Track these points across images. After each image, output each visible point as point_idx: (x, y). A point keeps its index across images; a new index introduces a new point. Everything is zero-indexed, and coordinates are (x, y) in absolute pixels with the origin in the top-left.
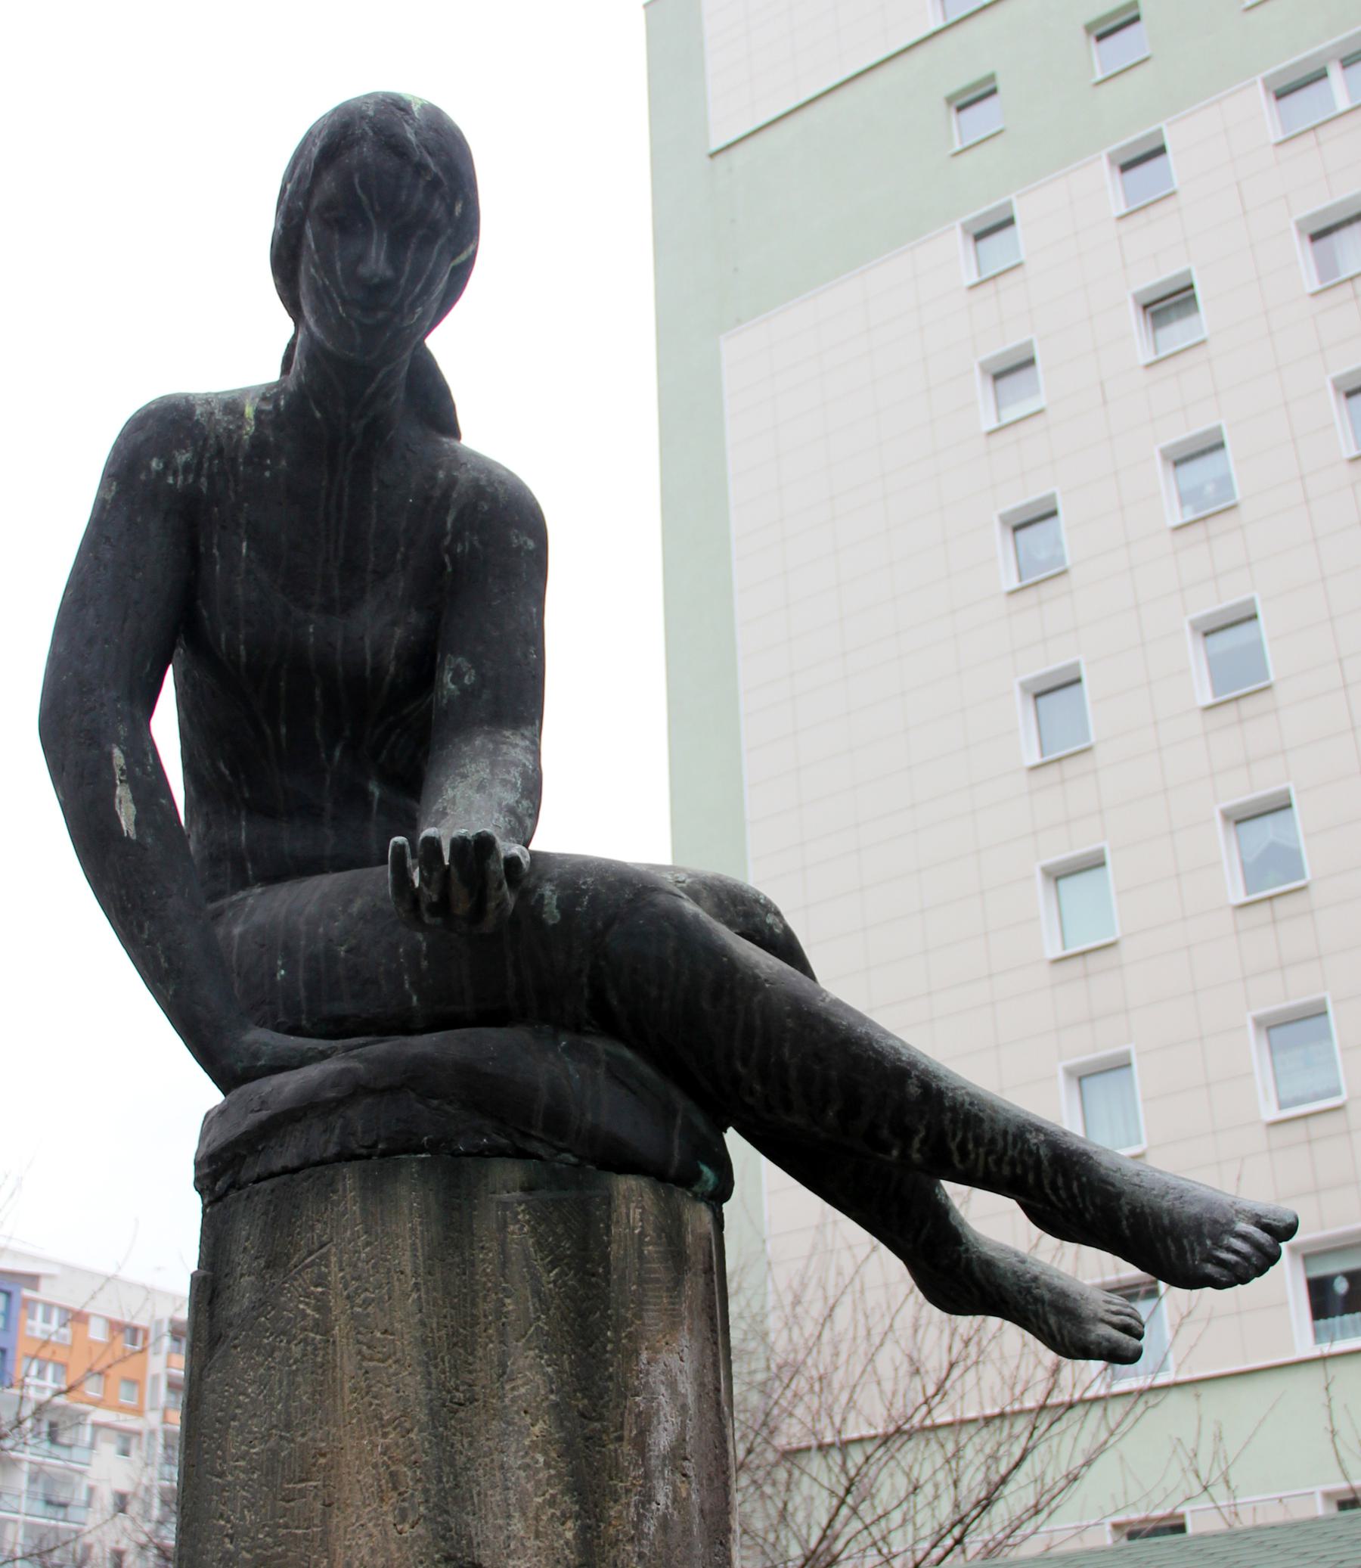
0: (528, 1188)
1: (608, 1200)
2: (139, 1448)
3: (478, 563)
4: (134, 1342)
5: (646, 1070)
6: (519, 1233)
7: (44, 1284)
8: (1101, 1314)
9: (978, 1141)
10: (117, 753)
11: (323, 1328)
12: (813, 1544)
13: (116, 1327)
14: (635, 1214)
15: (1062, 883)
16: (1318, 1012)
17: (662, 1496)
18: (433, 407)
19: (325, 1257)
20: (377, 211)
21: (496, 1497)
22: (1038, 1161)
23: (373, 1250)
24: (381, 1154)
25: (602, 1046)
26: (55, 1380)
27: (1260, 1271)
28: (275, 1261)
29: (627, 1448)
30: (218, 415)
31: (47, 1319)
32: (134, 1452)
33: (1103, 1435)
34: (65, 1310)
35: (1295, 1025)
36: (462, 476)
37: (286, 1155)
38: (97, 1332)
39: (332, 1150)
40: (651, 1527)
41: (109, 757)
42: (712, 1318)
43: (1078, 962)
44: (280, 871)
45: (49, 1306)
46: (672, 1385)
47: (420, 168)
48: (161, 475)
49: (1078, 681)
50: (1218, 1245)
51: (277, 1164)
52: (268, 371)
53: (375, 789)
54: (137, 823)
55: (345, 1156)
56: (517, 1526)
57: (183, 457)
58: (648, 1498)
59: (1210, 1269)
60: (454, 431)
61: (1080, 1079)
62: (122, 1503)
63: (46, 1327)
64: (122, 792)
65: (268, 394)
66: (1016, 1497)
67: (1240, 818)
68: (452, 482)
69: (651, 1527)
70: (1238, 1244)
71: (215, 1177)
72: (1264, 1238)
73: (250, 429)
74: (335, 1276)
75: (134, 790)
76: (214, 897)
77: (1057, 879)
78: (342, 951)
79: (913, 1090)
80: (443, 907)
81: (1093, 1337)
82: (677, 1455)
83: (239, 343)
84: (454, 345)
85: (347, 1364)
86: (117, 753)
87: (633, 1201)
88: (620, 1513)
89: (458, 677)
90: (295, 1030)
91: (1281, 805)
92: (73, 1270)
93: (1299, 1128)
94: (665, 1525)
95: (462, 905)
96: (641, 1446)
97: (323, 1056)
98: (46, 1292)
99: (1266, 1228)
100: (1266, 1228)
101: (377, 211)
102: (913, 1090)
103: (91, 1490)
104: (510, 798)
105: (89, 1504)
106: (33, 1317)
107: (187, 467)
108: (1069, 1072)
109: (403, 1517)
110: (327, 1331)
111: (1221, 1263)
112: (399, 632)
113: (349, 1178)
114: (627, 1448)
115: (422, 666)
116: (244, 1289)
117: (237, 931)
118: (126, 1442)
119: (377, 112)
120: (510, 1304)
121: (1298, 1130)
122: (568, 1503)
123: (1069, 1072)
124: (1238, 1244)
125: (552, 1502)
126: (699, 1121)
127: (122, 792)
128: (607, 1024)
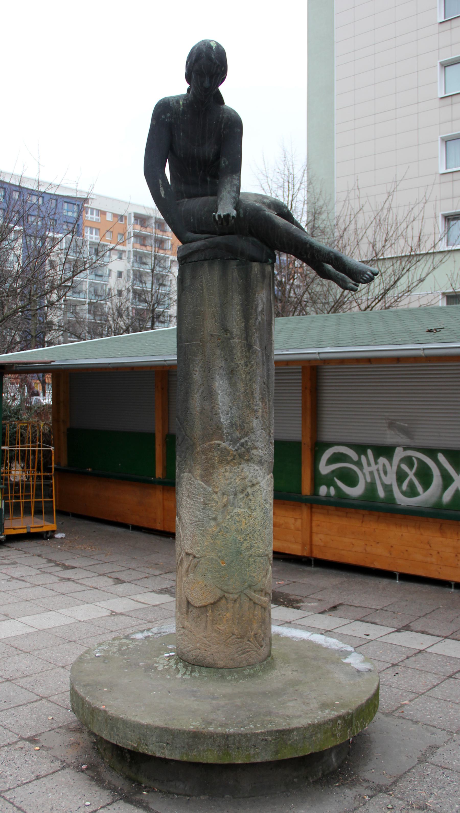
0: (237, 266)
1: (251, 267)
2: (125, 256)
3: (228, 132)
4: (122, 221)
5: (259, 242)
6: (235, 274)
7: (90, 201)
9: (320, 255)
10: (160, 181)
11: (202, 290)
12: (338, 297)
13: (115, 215)
14: (256, 269)
15: (447, 68)
17: (259, 319)
18: (219, 99)
19: (202, 278)
20: (207, 66)
21: (231, 319)
22: (332, 259)
23: (210, 278)
24: (211, 260)
25: (251, 238)
26: (96, 234)
28: (193, 277)
29: (253, 311)
30: (175, 104)
31: (92, 214)
32: (123, 258)
33: (431, 268)
34: (98, 211)
36: (225, 116)
37: (195, 258)
38: (109, 217)
39: (203, 258)
40: (257, 324)
41: (159, 182)
42: (270, 286)
43: (450, 99)
44: (190, 196)
45: (92, 209)
46: (262, 299)
47: (215, 63)
48: (164, 119)
50: (363, 276)
51: (193, 260)
52: (185, 92)
53: (209, 179)
54: (165, 195)
55: (205, 260)
56: (234, 324)
57: (168, 115)
58: (257, 319)
59: (361, 280)
60: (223, 103)
61: (446, 142)
62: (120, 274)
63: (92, 216)
64: (161, 188)
65: (185, 97)
66: (403, 284)
68: (223, 117)
69: (257, 324)
70: (367, 276)
71: (182, 261)
73: (182, 108)
74: (204, 281)
75: (164, 188)
76: (178, 200)
77: (445, 67)
78: (203, 218)
79: (308, 246)
80: (222, 224)
82: (262, 311)
83: (179, 87)
84: (222, 88)
85: (206, 296)
86: (160, 181)
87: (256, 267)
88: (252, 321)
89: (224, 163)
90: (195, 232)
92: (100, 196)
94: (260, 323)
95: (225, 224)
96: (256, 310)
97: (201, 239)
98: (91, 204)
101: (207, 66)
102: (308, 246)
103: (110, 271)
104: (234, 194)
105: (109, 275)
106: (87, 213)
107: (169, 117)
108: (442, 139)
109: (216, 322)
110: (203, 291)
111: (363, 279)
112: (213, 150)
113: (206, 264)
114: (253, 311)
115: (218, 156)
116: (188, 282)
117: (183, 209)
118: (121, 254)
119: (206, 50)
120: (234, 286)
122: (243, 320)
123: (442, 139)
124: (367, 276)
125: (240, 320)
126: (269, 251)
127: (161, 188)
128: (252, 234)
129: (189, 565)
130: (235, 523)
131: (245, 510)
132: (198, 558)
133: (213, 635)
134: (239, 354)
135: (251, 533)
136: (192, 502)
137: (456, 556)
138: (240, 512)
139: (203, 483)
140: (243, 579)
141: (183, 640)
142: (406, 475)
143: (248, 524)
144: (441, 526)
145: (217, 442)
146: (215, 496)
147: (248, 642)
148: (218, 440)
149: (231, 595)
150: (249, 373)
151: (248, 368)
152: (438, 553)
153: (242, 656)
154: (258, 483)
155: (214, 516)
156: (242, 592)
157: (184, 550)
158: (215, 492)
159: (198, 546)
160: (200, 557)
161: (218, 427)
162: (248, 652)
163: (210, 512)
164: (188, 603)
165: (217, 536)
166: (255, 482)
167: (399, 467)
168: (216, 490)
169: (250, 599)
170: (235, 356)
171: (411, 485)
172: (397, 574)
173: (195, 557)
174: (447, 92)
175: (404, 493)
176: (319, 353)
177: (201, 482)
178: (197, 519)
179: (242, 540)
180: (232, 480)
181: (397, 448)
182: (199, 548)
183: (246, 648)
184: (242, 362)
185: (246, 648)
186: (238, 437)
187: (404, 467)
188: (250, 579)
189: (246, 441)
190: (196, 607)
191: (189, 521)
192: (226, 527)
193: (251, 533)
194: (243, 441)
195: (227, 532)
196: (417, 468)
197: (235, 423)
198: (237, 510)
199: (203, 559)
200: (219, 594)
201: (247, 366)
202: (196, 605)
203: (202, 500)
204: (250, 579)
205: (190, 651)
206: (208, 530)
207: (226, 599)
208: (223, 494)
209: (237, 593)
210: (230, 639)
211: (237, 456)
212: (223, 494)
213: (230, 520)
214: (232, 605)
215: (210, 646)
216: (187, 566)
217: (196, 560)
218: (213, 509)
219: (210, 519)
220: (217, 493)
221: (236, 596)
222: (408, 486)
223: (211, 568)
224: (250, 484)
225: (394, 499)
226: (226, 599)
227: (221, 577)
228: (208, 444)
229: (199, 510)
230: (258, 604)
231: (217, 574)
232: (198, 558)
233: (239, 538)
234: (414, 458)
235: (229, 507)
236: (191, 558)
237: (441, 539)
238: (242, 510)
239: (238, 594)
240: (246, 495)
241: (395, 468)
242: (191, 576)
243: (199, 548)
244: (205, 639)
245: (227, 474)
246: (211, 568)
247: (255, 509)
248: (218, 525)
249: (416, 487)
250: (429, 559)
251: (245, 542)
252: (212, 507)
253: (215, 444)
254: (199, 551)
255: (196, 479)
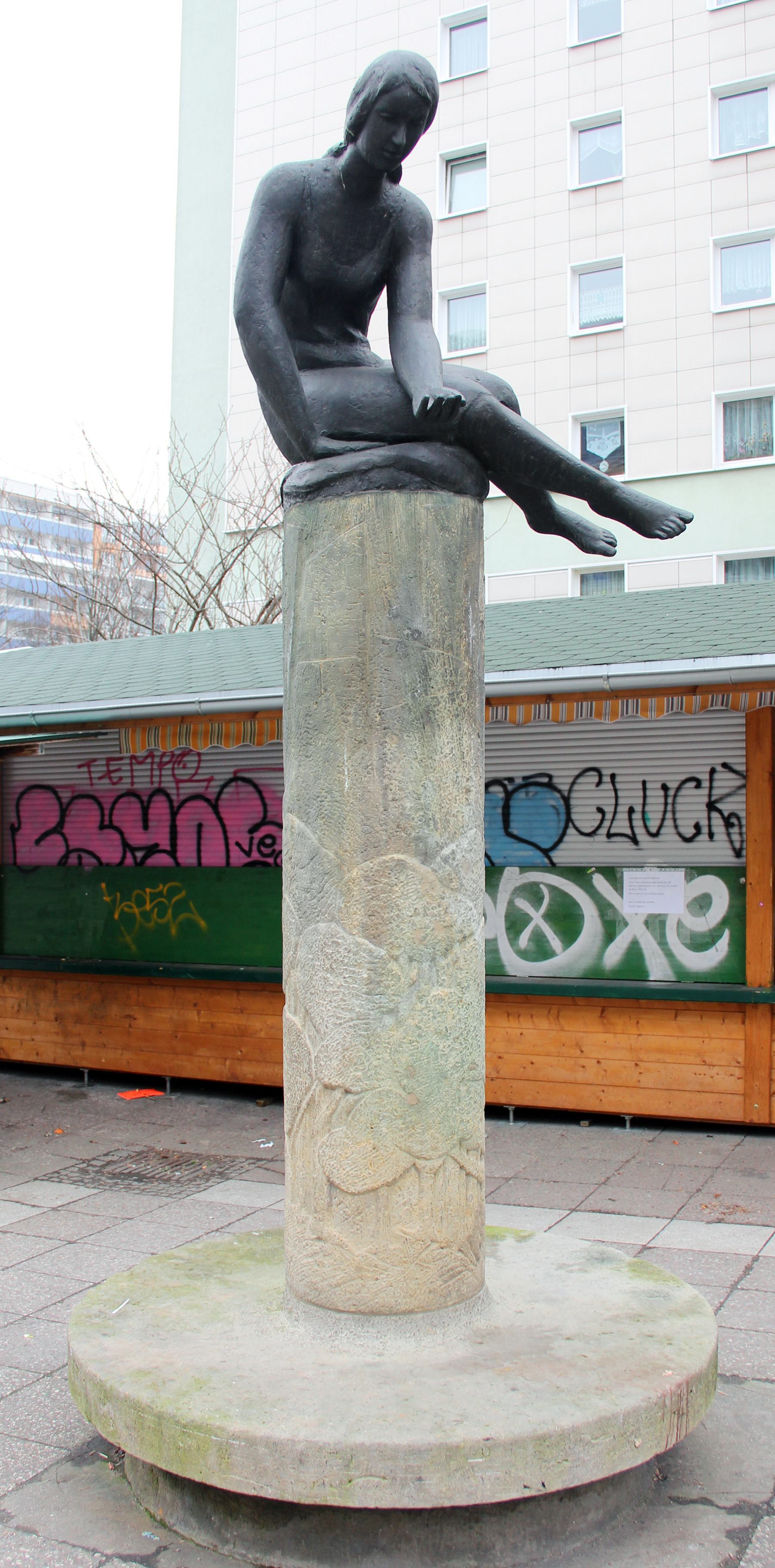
8: (602, 537)
16: (616, 266)
20: (395, 112)
27: (678, 534)
35: (599, 271)
49: (485, 20)
67: (583, 129)
72: (681, 523)
81: (598, 546)
91: (615, 122)
93: (591, 342)
99: (681, 519)
100: (681, 519)
121: (590, 343)
129: (334, 1111)
130: (434, 1017)
131: (452, 990)
132: (357, 1093)
133: (391, 1247)
134: (439, 679)
135: (462, 1034)
136: (340, 981)
137: (637, 1065)
138: (443, 995)
139: (367, 942)
140: (451, 1127)
141: (320, 1264)
142: (526, 919)
143: (458, 1017)
144: (603, 1012)
145: (396, 856)
146: (393, 966)
147: (460, 1254)
148: (398, 852)
149: (428, 1163)
150: (458, 715)
151: (455, 707)
152: (598, 1062)
153: (450, 1283)
154: (472, 934)
155: (392, 1005)
156: (447, 1154)
157: (320, 1080)
158: (392, 957)
159: (356, 1070)
160: (362, 1092)
161: (398, 827)
162: (460, 1273)
163: (384, 1000)
164: (331, 1184)
165: (400, 1046)
166: (467, 933)
167: (511, 903)
168: (396, 952)
169: (462, 1168)
170: (432, 683)
171: (538, 938)
172: (511, 1108)
173: (347, 1092)
174: (453, 210)
175: (524, 954)
176: (34, 715)
177: (361, 940)
178: (354, 1015)
179: (447, 1050)
180: (428, 931)
181: (507, 868)
182: (359, 1073)
183: (456, 1267)
184: (445, 694)
185: (456, 1267)
186: (437, 843)
187: (523, 904)
188: (462, 1127)
189: (453, 852)
190: (353, 1194)
191: (333, 1020)
192: (417, 1026)
193: (462, 1034)
194: (446, 851)
195: (420, 1036)
196: (550, 905)
197: (433, 816)
198: (436, 991)
199: (367, 1096)
200: (405, 1161)
201: (453, 700)
202: (352, 1189)
203: (365, 976)
204: (462, 1127)
205: (339, 1285)
206: (379, 1036)
207: (417, 1170)
208: (411, 959)
209: (440, 1157)
210: (426, 1252)
211: (437, 882)
212: (411, 959)
213: (425, 1011)
214: (431, 1182)
215: (386, 1270)
216: (328, 1113)
217: (350, 1097)
218: (390, 992)
219: (383, 1013)
220: (396, 959)
221: (437, 1163)
222: (530, 940)
223: (387, 1111)
224: (459, 936)
225: (502, 966)
226: (417, 1170)
227: (408, 1128)
228: (377, 860)
229: (357, 996)
230: (473, 1176)
231: (401, 1122)
232: (357, 1093)
233: (441, 1047)
234: (542, 886)
235: (422, 985)
236: (338, 1094)
237: (602, 1037)
238: (446, 990)
239: (442, 1159)
240: (452, 960)
241: (502, 907)
242: (340, 1131)
243: (359, 1073)
244: (374, 1257)
245: (417, 919)
246: (387, 1111)
247: (468, 986)
248: (399, 1023)
249: (548, 941)
250: (580, 1076)
251: (454, 1053)
252: (387, 987)
253: (393, 860)
254: (359, 1080)
255: (351, 934)
